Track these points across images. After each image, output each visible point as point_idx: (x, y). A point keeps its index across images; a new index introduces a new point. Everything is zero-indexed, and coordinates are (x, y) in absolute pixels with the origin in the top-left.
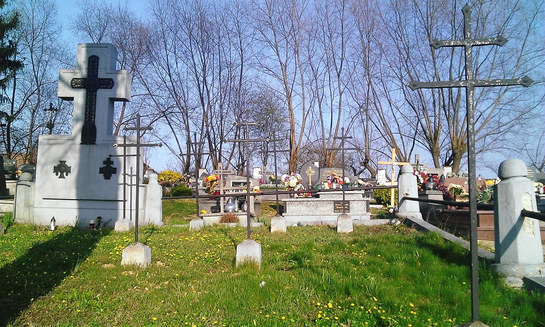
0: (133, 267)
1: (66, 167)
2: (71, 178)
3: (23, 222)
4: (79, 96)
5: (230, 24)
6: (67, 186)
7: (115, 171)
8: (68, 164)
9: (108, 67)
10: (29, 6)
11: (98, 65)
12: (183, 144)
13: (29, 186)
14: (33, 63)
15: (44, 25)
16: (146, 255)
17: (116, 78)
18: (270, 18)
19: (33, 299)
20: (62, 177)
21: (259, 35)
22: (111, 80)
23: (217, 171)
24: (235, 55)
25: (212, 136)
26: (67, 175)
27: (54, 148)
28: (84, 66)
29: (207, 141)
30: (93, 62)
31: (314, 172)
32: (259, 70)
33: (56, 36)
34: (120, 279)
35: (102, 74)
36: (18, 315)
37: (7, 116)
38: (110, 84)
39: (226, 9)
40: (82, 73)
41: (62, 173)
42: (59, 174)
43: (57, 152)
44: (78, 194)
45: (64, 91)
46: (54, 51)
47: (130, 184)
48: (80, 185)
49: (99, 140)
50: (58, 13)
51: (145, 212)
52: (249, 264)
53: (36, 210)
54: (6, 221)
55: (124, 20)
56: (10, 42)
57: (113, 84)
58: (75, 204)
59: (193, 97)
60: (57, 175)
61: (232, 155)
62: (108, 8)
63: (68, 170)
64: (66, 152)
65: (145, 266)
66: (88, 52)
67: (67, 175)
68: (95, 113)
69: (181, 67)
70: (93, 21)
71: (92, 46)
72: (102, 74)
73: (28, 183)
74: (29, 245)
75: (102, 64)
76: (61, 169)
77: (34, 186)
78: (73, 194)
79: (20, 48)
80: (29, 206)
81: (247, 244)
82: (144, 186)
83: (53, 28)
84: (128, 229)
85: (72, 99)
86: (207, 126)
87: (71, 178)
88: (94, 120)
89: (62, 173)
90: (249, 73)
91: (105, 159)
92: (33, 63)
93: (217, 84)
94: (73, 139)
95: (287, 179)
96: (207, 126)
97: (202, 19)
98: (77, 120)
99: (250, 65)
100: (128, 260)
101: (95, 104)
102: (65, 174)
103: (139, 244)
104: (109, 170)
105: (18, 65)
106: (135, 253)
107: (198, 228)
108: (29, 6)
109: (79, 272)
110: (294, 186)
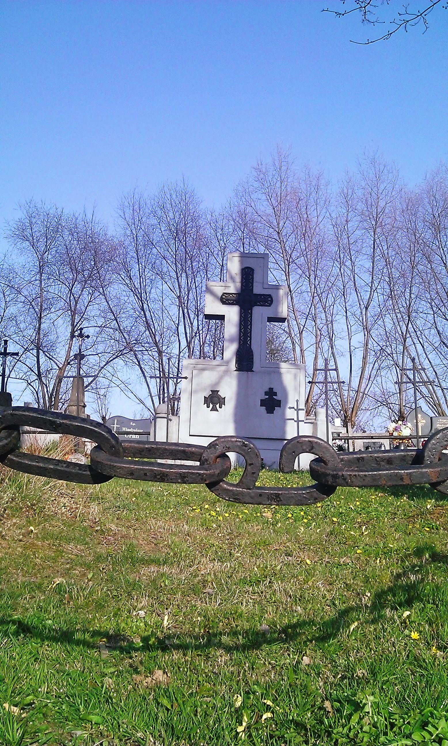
1: (219, 397)
4: (232, 314)
7: (278, 404)
8: (221, 394)
11: (253, 278)
14: (159, 370)
17: (277, 294)
20: (214, 409)
22: (270, 296)
26: (220, 407)
27: (206, 373)
28: (238, 279)
30: (247, 274)
31: (424, 421)
35: (257, 289)
38: (267, 300)
40: (233, 288)
41: (214, 404)
42: (211, 406)
43: (207, 379)
45: (213, 307)
47: (296, 419)
49: (256, 366)
57: (272, 301)
60: (208, 407)
63: (222, 401)
64: (221, 378)
66: (241, 262)
67: (220, 407)
70: (38, 229)
71: (255, 256)
72: (257, 289)
75: (257, 277)
76: (214, 400)
85: (221, 318)
87: (228, 409)
88: (250, 342)
89: (214, 404)
91: (267, 390)
94: (228, 362)
98: (231, 341)
101: (251, 324)
102: (218, 406)
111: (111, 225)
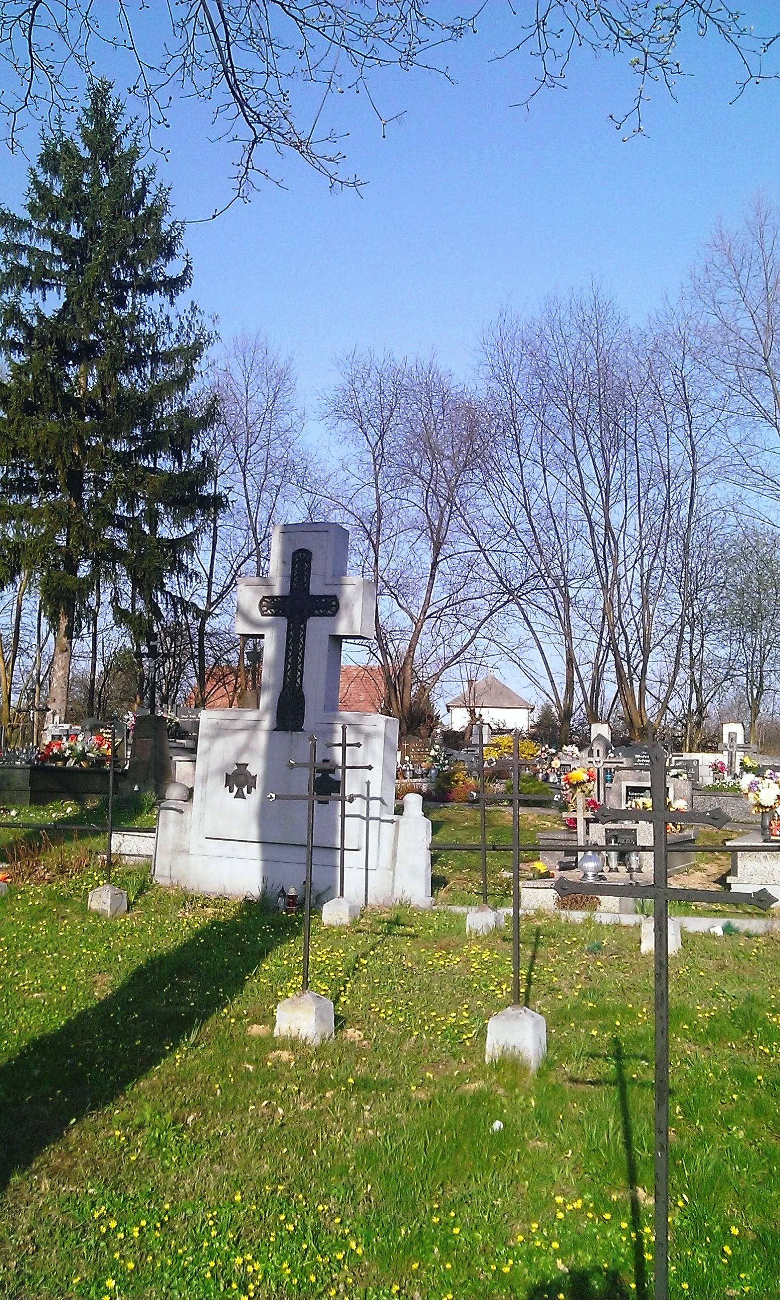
0: (293, 1043)
2: (254, 798)
5: (667, 383)
9: (329, 572)
12: (559, 665)
13: (181, 812)
14: (246, 497)
15: (272, 409)
16: (320, 1018)
18: (766, 360)
20: (239, 795)
21: (738, 402)
23: (591, 759)
25: (622, 648)
26: (249, 792)
29: (611, 657)
33: (292, 435)
34: (261, 1069)
35: (316, 588)
36: (40, 1153)
38: (330, 606)
41: (240, 787)
46: (289, 468)
52: (510, 1064)
53: (192, 858)
56: (204, 454)
57: (337, 606)
59: (581, 556)
60: (231, 791)
61: (672, 684)
65: (318, 1041)
67: (249, 792)
69: (554, 489)
72: (316, 588)
73: (180, 805)
74: (134, 968)
76: (238, 779)
80: (181, 851)
81: (509, 1018)
82: (392, 821)
83: (285, 421)
84: (346, 920)
87: (254, 798)
88: (301, 680)
89: (240, 787)
90: (717, 492)
92: (246, 497)
93: (633, 522)
97: (603, 372)
99: (723, 474)
100: (287, 1027)
102: (245, 790)
103: (308, 996)
105: (217, 503)
107: (484, 931)
108: (239, 377)
109: (196, 1045)
110: (772, 804)
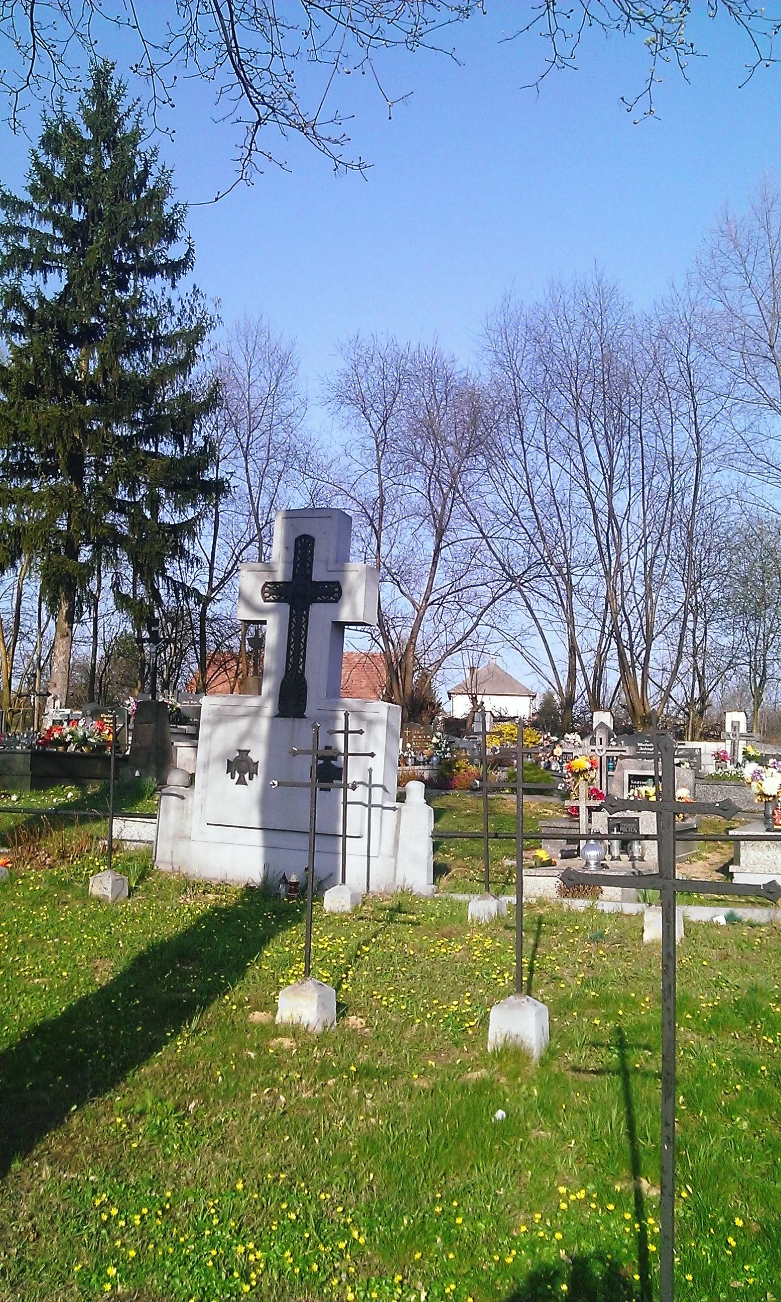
0: (295, 1031)
2: (256, 784)
3: (169, 868)
5: (672, 371)
6: (243, 800)
9: (332, 557)
10: (241, 362)
11: (312, 554)
12: (561, 653)
13: (183, 798)
14: (248, 482)
15: (273, 395)
16: (322, 1005)
19: (75, 1107)
20: (241, 782)
21: (743, 389)
23: (593, 748)
24: (682, 440)
25: (625, 636)
26: (251, 778)
29: (614, 645)
32: (747, 473)
33: (294, 420)
34: (263, 1056)
35: (319, 574)
37: (199, 595)
38: (333, 592)
39: (663, 336)
42: (237, 775)
44: (263, 822)
46: (291, 453)
48: (266, 802)
50: (300, 372)
51: (396, 862)
52: (512, 1053)
53: (193, 844)
54: (135, 868)
55: (433, 373)
56: (205, 438)
57: (340, 593)
58: (257, 837)
59: (584, 543)
60: (233, 778)
62: (402, 352)
65: (319, 1028)
67: (251, 778)
68: (304, 653)
69: (558, 475)
71: (317, 514)
72: (319, 574)
75: (322, 552)
76: (240, 766)
77: (192, 796)
78: (255, 819)
79: (225, 449)
81: (512, 1006)
82: (394, 809)
83: (286, 406)
84: (348, 908)
86: (615, 614)
87: (256, 784)
88: (304, 667)
90: (721, 480)
95: (756, 775)
96: (615, 614)
97: (607, 359)
102: (247, 776)
104: (329, 772)
105: (219, 488)
106: (301, 1001)
107: (485, 919)
108: (241, 362)
111: (471, 360)
